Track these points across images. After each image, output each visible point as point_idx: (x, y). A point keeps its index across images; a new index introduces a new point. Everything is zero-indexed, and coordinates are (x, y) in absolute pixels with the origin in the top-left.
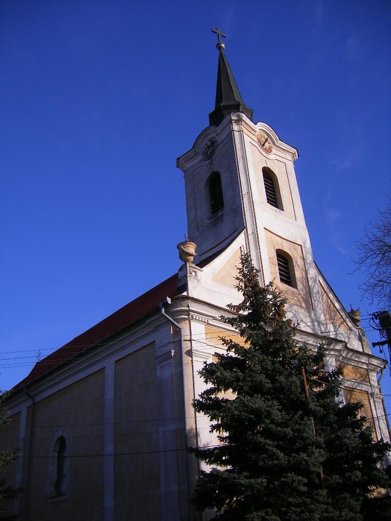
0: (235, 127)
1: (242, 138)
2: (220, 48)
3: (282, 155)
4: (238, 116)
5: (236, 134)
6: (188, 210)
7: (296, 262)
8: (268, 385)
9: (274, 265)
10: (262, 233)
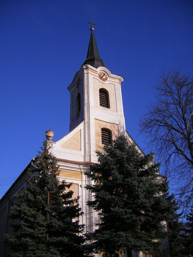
0: (85, 71)
1: (88, 76)
2: (91, 30)
3: (113, 80)
4: (86, 66)
5: (85, 75)
6: (71, 111)
7: (114, 133)
8: (32, 198)
9: (99, 136)
10: (92, 122)
